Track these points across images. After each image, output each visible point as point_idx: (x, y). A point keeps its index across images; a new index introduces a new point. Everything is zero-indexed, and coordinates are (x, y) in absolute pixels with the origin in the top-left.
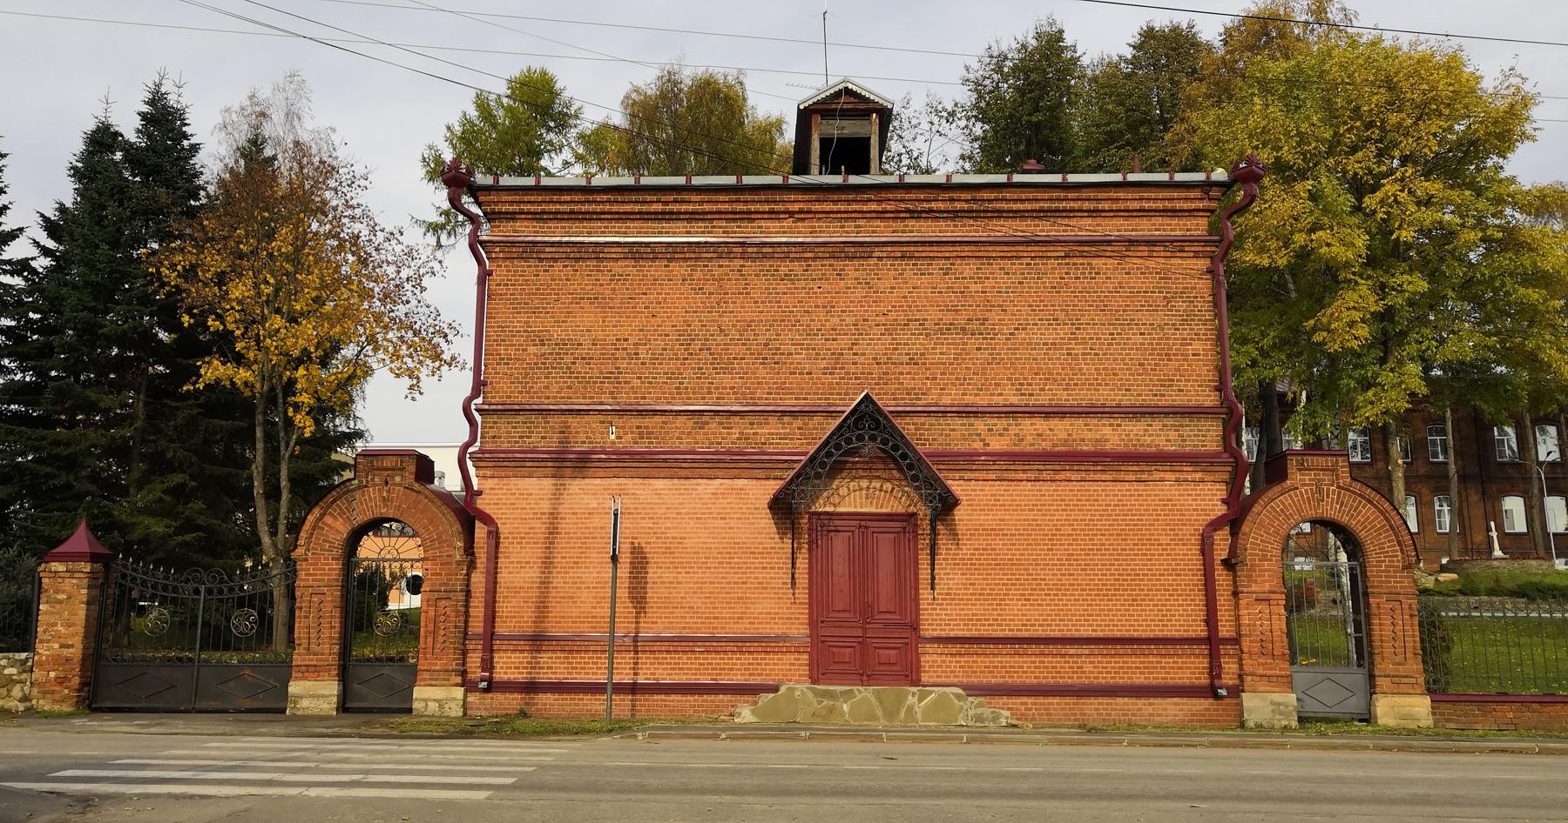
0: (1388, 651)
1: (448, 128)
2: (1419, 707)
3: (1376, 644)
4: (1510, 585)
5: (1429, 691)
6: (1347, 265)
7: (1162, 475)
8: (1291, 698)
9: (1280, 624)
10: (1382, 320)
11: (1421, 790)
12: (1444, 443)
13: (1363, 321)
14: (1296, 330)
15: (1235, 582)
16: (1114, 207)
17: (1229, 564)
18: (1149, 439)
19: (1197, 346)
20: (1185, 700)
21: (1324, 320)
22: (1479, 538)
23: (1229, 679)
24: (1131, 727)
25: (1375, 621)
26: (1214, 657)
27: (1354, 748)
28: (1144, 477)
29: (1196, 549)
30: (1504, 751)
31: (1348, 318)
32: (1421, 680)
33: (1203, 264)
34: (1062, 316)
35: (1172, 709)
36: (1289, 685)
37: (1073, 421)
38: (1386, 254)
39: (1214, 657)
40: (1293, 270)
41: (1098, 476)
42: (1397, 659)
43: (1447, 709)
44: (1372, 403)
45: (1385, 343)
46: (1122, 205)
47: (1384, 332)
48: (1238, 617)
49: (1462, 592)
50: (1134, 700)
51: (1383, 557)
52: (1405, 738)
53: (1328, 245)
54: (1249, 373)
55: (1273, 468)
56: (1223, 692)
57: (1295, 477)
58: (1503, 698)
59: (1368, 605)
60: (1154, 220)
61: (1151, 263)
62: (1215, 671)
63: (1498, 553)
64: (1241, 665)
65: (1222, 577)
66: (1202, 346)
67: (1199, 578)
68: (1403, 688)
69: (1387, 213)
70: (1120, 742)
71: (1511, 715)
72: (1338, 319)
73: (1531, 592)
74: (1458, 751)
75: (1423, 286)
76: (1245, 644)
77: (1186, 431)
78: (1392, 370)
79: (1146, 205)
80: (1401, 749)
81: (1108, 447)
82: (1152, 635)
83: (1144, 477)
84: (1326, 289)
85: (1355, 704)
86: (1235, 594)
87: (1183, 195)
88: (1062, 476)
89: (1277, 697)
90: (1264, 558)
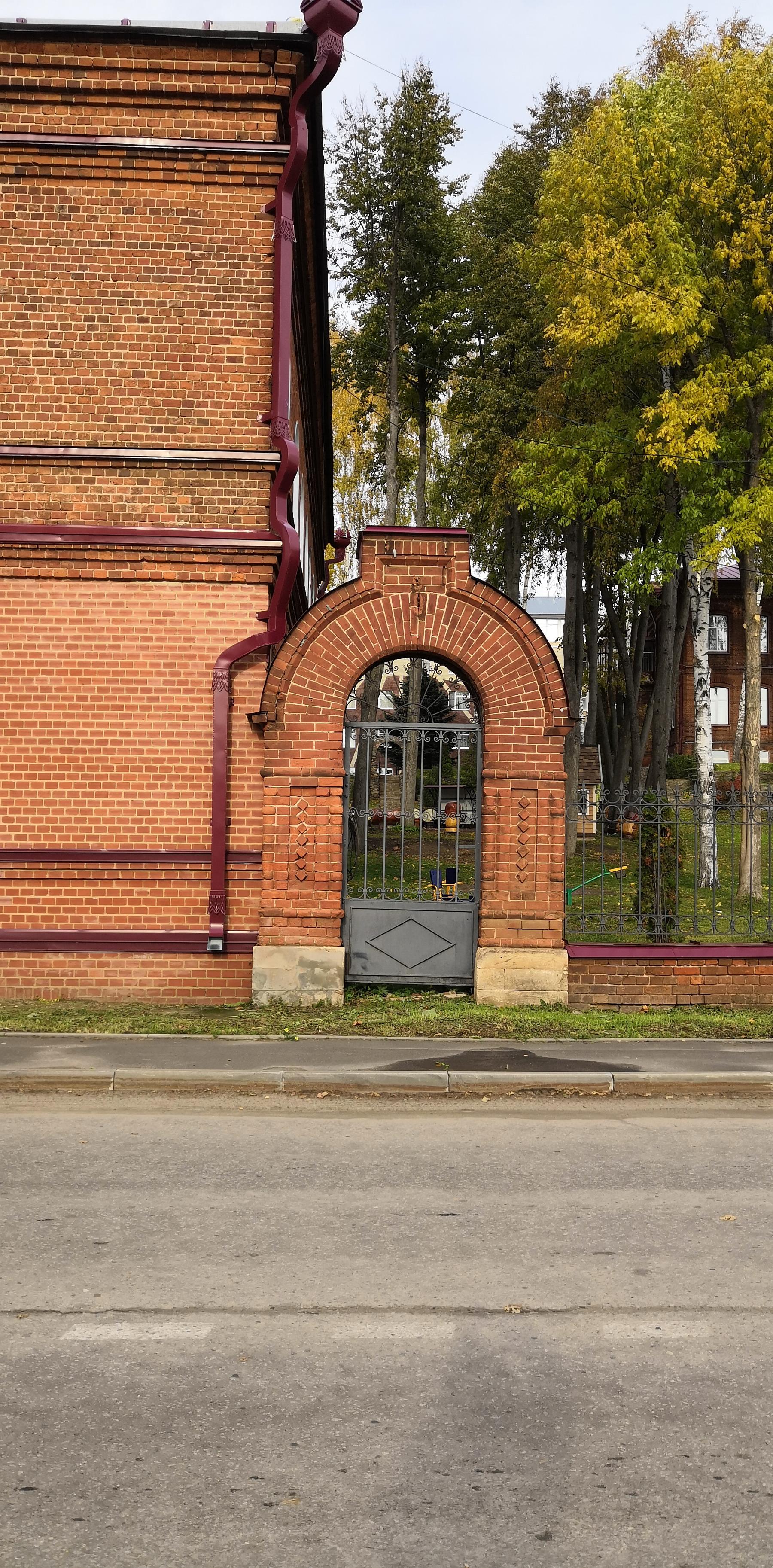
1: (692, 21)
2: (547, 970)
7: (157, 569)
8: (337, 955)
11: (244, 1101)
16: (107, 84)
18: (139, 506)
19: (239, 344)
20: (162, 958)
26: (220, 883)
28: (126, 571)
32: (557, 923)
33: (261, 198)
35: (138, 974)
39: (220, 883)
42: (524, 888)
43: (595, 971)
46: (119, 82)
60: (181, 115)
61: (172, 193)
62: (219, 908)
71: (699, 980)
77: (206, 494)
79: (164, 83)
81: (69, 520)
83: (126, 571)
85: (446, 966)
87: (229, 65)
89: (311, 953)
90: (313, 715)
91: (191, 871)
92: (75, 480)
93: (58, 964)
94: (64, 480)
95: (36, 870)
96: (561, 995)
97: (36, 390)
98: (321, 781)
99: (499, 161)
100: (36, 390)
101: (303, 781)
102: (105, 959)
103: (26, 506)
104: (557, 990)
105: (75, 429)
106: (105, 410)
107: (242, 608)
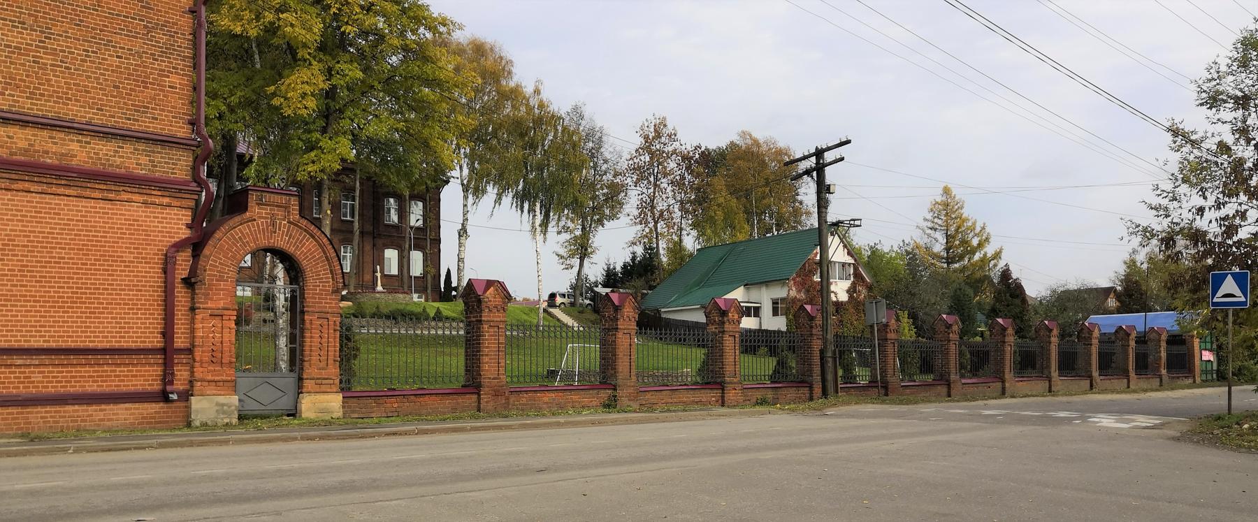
0: (315, 358)
2: (333, 402)
3: (307, 353)
4: (385, 311)
5: (342, 390)
6: (305, 46)
7: (130, 196)
9: (230, 336)
10: (327, 97)
11: (347, 477)
12: (353, 207)
13: (313, 95)
14: (259, 93)
15: (193, 299)
17: (189, 283)
18: (118, 160)
19: (174, 79)
20: (137, 405)
21: (283, 88)
22: (368, 277)
23: (179, 385)
24: (80, 433)
25: (307, 334)
26: (168, 365)
27: (286, 440)
28: (111, 196)
29: (158, 269)
30: (395, 434)
31: (301, 90)
34: (30, 21)
35: (123, 413)
36: (233, 387)
37: (36, 131)
38: (333, 44)
39: (168, 365)
40: (261, 42)
41: (61, 190)
44: (313, 162)
45: (327, 117)
47: (328, 108)
48: (193, 330)
49: (355, 316)
50: (85, 407)
51: (318, 282)
52: (325, 428)
53: (292, 25)
54: (217, 123)
55: (236, 204)
56: (175, 397)
57: (254, 210)
58: (392, 393)
59: (303, 321)
63: (379, 288)
64: (192, 373)
65: (181, 295)
66: (179, 81)
67: (158, 294)
68: (324, 388)
69: (339, 9)
70: (65, 450)
72: (294, 90)
73: (396, 316)
74: (363, 437)
75: (360, 75)
76: (198, 354)
78: (330, 139)
80: (322, 438)
81: (74, 162)
82: (108, 346)
83: (111, 196)
84: (285, 65)
85: (285, 403)
86: (193, 309)
88: (20, 186)
89: (221, 399)
90: (221, 279)
91: (151, 358)
92: (78, 141)
93: (74, 411)
94: (72, 141)
95: (63, 359)
96: (340, 414)
97: (53, 86)
98: (226, 312)
99: (480, 49)
100: (53, 86)
101: (217, 312)
102: (103, 407)
103: (47, 152)
104: (338, 413)
105: (76, 112)
106: (96, 104)
107: (174, 222)
